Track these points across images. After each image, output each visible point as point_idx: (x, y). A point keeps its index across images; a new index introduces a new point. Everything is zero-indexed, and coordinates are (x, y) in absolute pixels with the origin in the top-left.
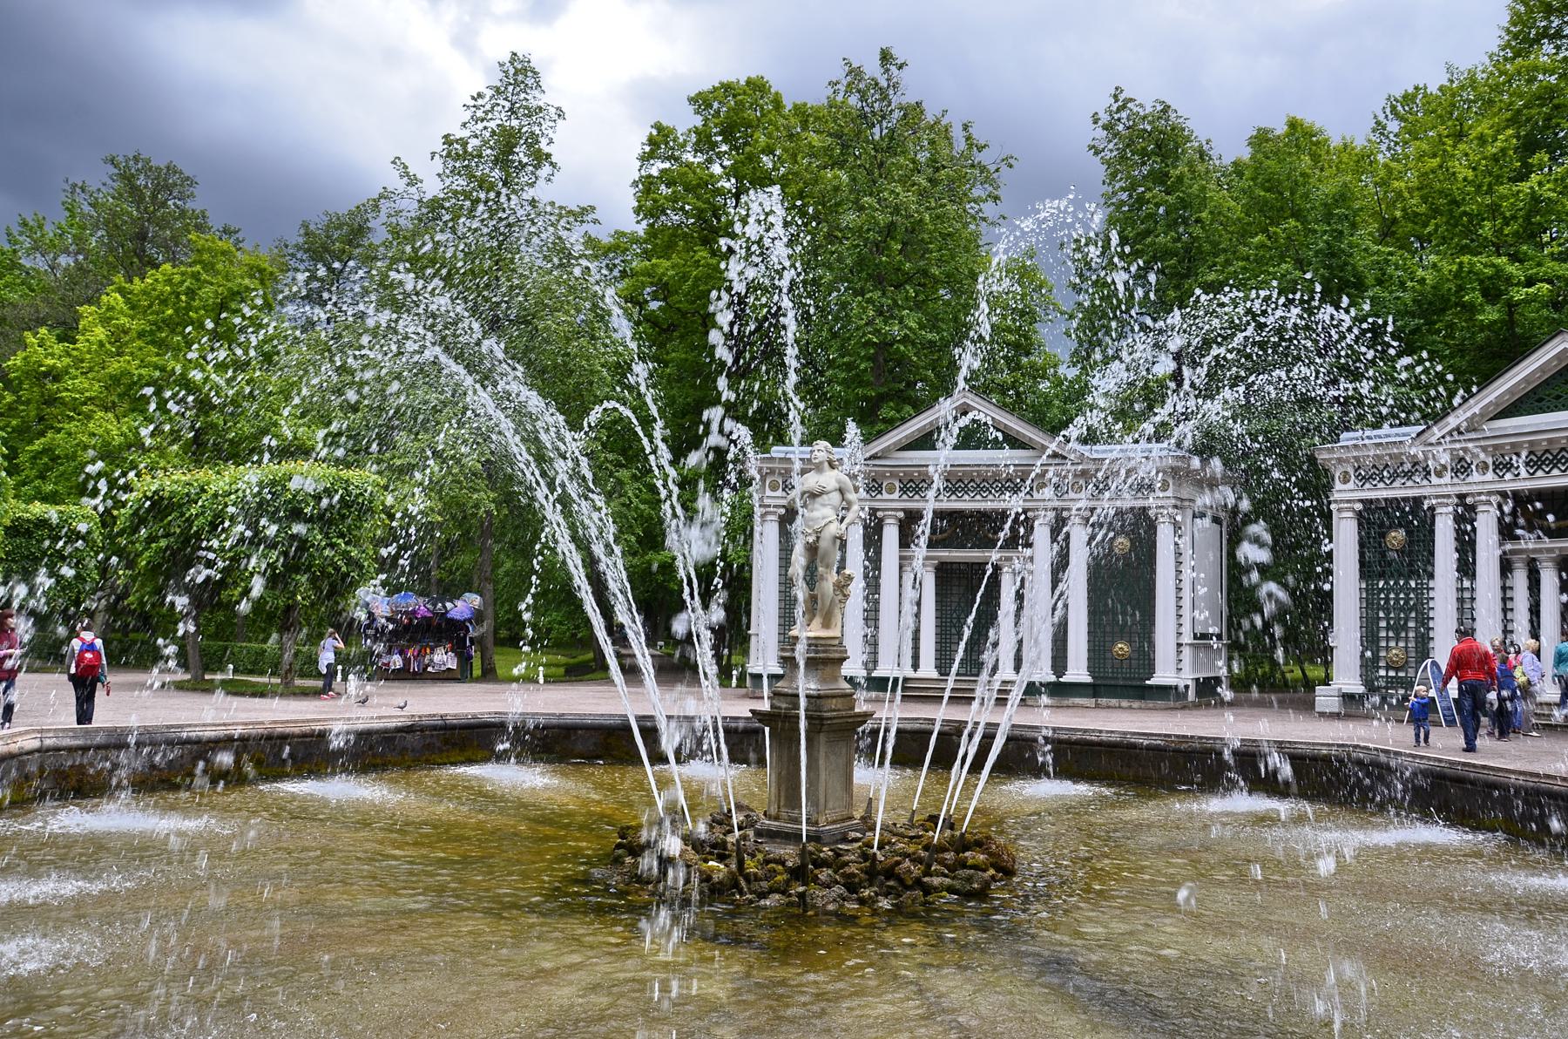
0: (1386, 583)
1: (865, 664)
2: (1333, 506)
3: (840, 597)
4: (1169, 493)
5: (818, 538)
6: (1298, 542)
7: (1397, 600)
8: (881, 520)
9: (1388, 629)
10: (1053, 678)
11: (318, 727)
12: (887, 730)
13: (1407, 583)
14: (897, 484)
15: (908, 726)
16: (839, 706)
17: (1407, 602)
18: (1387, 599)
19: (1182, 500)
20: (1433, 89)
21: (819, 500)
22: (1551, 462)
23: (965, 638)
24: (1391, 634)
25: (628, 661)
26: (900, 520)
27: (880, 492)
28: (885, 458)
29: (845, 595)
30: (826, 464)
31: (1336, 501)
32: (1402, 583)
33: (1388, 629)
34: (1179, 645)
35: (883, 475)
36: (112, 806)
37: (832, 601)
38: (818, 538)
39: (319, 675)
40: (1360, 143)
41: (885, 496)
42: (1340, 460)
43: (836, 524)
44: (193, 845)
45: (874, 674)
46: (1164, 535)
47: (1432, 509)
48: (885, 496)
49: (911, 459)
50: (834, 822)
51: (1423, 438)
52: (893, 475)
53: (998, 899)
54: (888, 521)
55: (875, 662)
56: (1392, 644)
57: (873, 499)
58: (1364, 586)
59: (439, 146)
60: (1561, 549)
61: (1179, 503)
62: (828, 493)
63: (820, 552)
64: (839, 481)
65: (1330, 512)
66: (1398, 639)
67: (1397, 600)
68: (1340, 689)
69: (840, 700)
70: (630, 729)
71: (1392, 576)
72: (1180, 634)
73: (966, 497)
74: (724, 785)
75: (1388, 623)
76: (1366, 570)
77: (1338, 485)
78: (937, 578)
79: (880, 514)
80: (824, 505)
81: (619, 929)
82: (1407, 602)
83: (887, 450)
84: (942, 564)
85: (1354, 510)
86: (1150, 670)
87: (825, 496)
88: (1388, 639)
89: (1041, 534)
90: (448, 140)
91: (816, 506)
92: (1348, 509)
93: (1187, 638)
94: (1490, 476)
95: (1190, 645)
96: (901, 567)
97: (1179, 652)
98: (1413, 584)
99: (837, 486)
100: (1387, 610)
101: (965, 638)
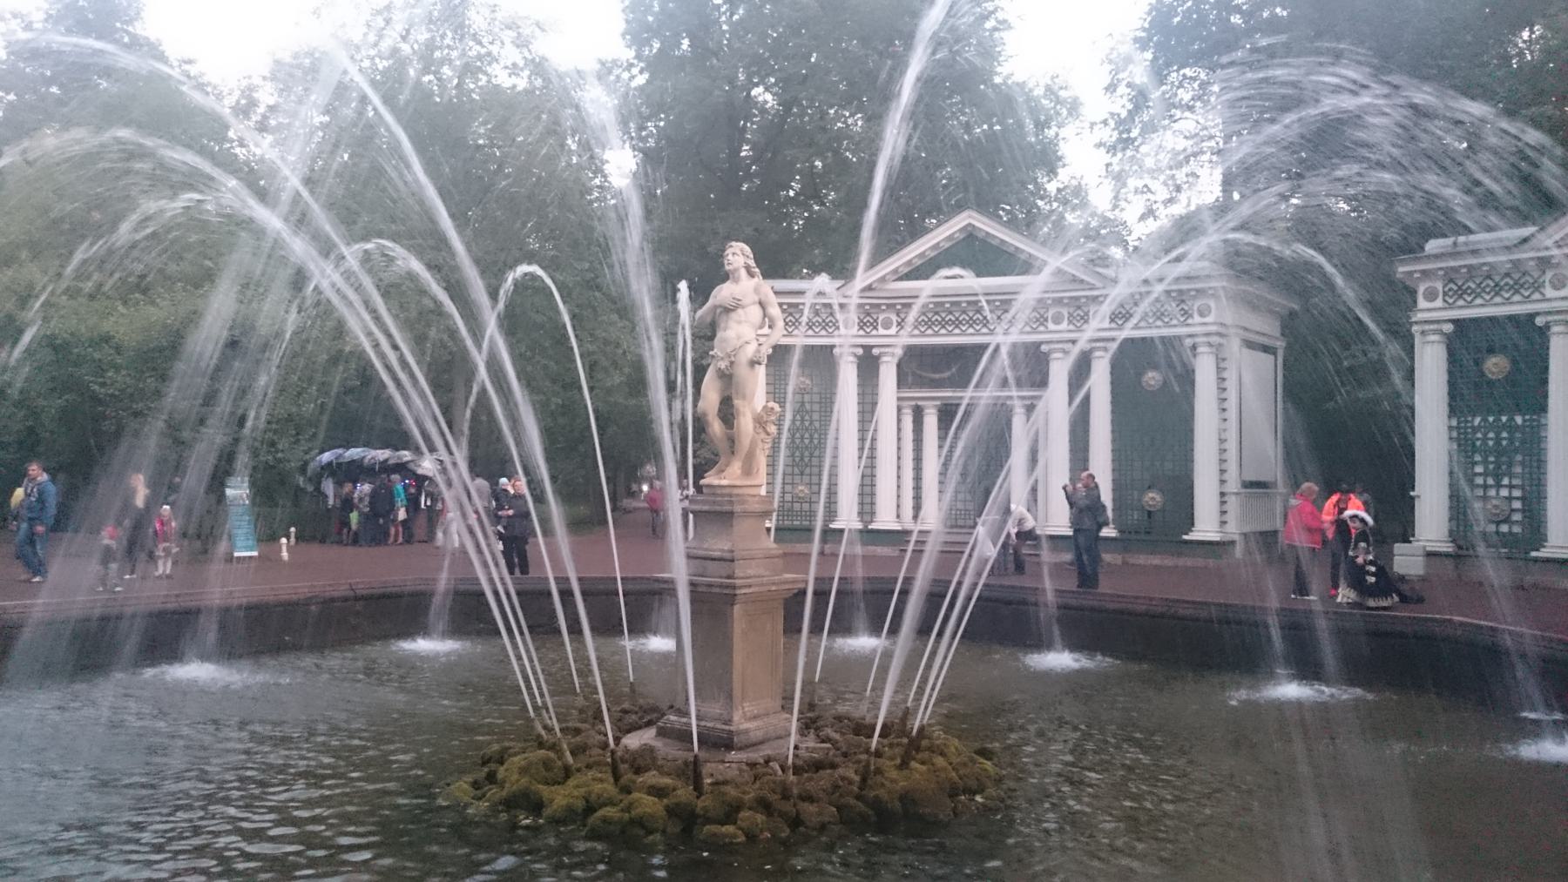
0: (1485, 420)
1: (861, 514)
2: (1415, 328)
8: (877, 358)
9: (1485, 474)
12: (905, 593)
13: (1511, 419)
15: (462, 588)
17: (802, 459)
18: (1485, 439)
21: (733, 315)
24: (1490, 481)
25: (583, 510)
27: (875, 328)
30: (743, 272)
31: (1416, 323)
32: (1504, 419)
33: (1485, 474)
34: (1222, 494)
36: (273, 662)
42: (1425, 274)
47: (1547, 326)
48: (881, 331)
50: (755, 717)
52: (889, 306)
53: (396, 762)
54: (1097, 354)
55: (873, 513)
56: (1492, 492)
57: (868, 335)
58: (1454, 423)
65: (1412, 337)
66: (1499, 486)
68: (1424, 547)
70: (593, 629)
71: (1489, 412)
72: (1223, 482)
73: (823, 333)
75: (1486, 468)
76: (1457, 403)
77: (1422, 303)
79: (875, 351)
80: (739, 322)
82: (802, 459)
85: (1441, 332)
86: (1190, 523)
87: (740, 311)
88: (1485, 487)
89: (1059, 371)
92: (1435, 332)
93: (1233, 485)
94: (1064, 325)
95: (1237, 494)
96: (899, 409)
97: (1223, 503)
98: (1519, 420)
100: (1486, 453)
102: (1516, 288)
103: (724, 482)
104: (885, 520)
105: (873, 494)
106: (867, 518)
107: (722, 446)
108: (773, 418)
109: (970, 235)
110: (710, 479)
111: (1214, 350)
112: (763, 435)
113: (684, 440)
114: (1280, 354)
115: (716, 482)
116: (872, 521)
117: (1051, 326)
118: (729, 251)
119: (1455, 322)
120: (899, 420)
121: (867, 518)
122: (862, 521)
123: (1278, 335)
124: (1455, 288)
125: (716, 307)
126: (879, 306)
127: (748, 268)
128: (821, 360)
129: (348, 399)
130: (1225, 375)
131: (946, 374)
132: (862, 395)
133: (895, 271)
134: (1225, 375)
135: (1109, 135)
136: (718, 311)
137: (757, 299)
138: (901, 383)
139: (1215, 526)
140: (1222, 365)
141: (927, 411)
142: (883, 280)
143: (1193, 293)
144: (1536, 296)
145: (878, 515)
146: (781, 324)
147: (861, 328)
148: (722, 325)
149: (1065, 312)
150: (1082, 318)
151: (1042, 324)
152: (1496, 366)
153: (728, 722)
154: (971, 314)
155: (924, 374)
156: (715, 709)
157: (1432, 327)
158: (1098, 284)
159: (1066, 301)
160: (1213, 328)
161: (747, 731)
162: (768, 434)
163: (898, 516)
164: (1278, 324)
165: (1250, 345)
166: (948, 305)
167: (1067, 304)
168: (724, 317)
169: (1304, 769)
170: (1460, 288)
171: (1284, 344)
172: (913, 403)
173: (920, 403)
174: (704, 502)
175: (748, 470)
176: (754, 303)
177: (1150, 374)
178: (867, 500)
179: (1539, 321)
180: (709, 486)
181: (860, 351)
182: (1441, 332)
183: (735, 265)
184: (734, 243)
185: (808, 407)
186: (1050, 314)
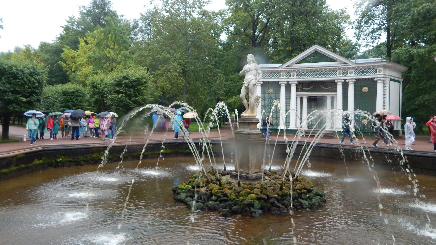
3: (256, 103)
4: (382, 73)
5: (249, 85)
6: (403, 211)
8: (291, 84)
11: (155, 132)
14: (295, 74)
16: (256, 137)
19: (386, 75)
21: (249, 73)
22: (366, 72)
23: (204, 119)
26: (261, 84)
27: (290, 76)
28: (292, 66)
29: (258, 103)
30: (252, 62)
35: (291, 71)
37: (254, 105)
38: (249, 85)
41: (292, 77)
42: (349, 68)
43: (254, 80)
45: (289, 128)
46: (380, 87)
48: (292, 77)
50: (254, 173)
51: (282, 67)
52: (294, 71)
55: (289, 125)
57: (288, 78)
61: (385, 76)
62: (251, 71)
63: (249, 89)
64: (255, 66)
69: (256, 135)
74: (213, 161)
79: (347, 81)
80: (251, 74)
83: (292, 64)
84: (309, 97)
85: (352, 81)
86: (278, 125)
91: (248, 75)
92: (339, 82)
96: (296, 98)
99: (255, 68)
101: (204, 119)
102: (276, 76)
103: (247, 115)
104: (292, 127)
105: (289, 120)
106: (287, 126)
109: (316, 53)
110: (243, 114)
111: (382, 81)
113: (248, 120)
114: (401, 83)
115: (244, 115)
117: (338, 75)
118: (248, 56)
119: (298, 81)
120: (296, 101)
123: (401, 77)
125: (245, 71)
126: (291, 70)
128: (277, 85)
129: (395, 51)
130: (385, 88)
132: (286, 94)
133: (295, 62)
134: (385, 88)
135: (356, 25)
136: (245, 71)
138: (297, 91)
140: (385, 86)
141: (304, 98)
143: (377, 66)
145: (290, 125)
146: (261, 75)
147: (286, 76)
148: (246, 75)
149: (342, 71)
150: (375, 71)
151: (335, 75)
152: (365, 89)
153: (248, 174)
154: (359, 70)
155: (303, 88)
156: (244, 171)
157: (351, 80)
158: (351, 64)
159: (352, 68)
160: (382, 76)
161: (252, 176)
163: (296, 126)
164: (401, 74)
165: (391, 80)
167: (342, 70)
168: (247, 73)
169: (271, 114)
170: (367, 71)
171: (402, 80)
172: (332, 96)
173: (333, 96)
174: (241, 120)
176: (254, 70)
177: (365, 88)
179: (375, 79)
180: (243, 116)
181: (343, 81)
182: (352, 81)
185: (272, 97)
186: (337, 72)
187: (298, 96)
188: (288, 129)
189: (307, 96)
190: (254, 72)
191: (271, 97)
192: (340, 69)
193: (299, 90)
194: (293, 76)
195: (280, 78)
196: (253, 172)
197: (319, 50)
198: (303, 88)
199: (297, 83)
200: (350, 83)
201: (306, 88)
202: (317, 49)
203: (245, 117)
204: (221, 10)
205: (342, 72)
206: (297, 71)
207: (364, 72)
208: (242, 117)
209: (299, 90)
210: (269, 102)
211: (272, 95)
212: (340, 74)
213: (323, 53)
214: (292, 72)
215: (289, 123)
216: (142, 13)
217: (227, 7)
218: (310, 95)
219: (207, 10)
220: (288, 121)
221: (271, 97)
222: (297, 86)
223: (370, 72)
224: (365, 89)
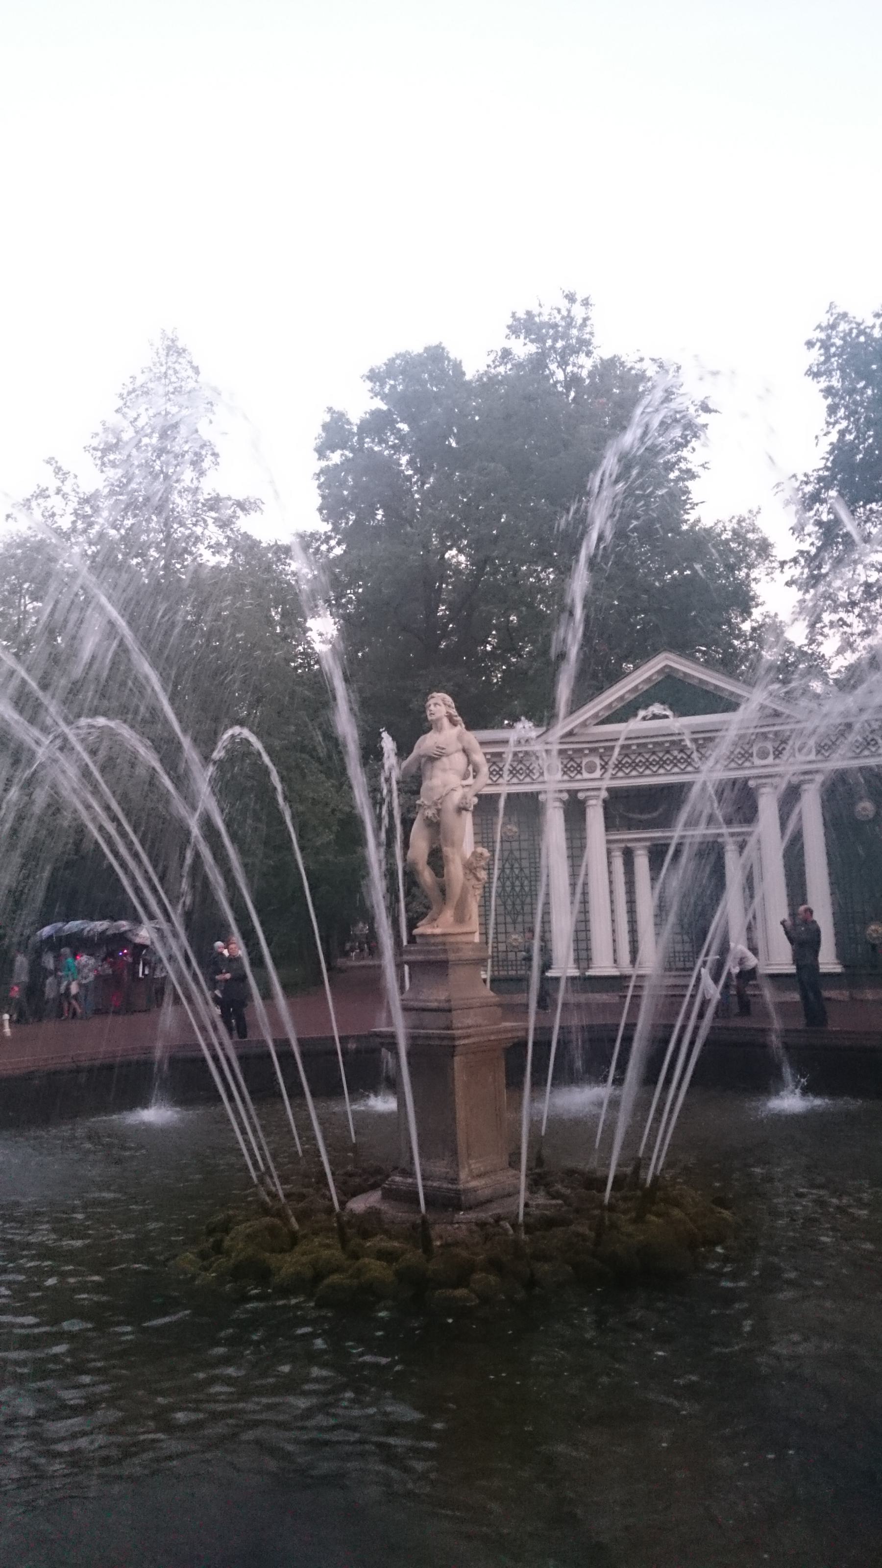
1: (577, 960)
5: (439, 811)
7: (513, 886)
10: (575, 973)
14: (598, 761)
20: (471, 372)
21: (438, 764)
27: (580, 772)
28: (582, 734)
30: (446, 721)
38: (439, 811)
39: (408, 963)
40: (774, 552)
44: (87, 1276)
45: (590, 973)
48: (586, 775)
49: (601, 734)
50: (480, 1176)
51: (543, 737)
55: (589, 959)
57: (572, 780)
59: (507, 331)
60: (654, 838)
64: (460, 738)
67: (513, 886)
78: (650, 861)
79: (581, 796)
80: (444, 770)
81: (86, 1379)
84: (656, 845)
87: (444, 759)
90: (509, 327)
96: (609, 852)
105: (588, 940)
106: (583, 964)
107: (434, 894)
108: (483, 863)
110: (424, 928)
112: (474, 882)
115: (429, 931)
116: (589, 968)
117: (757, 762)
118: (431, 702)
121: (583, 964)
122: (579, 968)
124: (575, 765)
126: (581, 750)
127: (450, 718)
131: (655, 814)
133: (596, 715)
137: (460, 746)
138: (610, 825)
139: (610, 962)
142: (584, 724)
144: (747, 764)
148: (428, 774)
150: (575, 769)
151: (747, 760)
155: (631, 815)
156: (440, 1167)
161: (475, 1190)
162: (478, 879)
163: (615, 961)
166: (650, 746)
172: (623, 845)
173: (629, 845)
175: (461, 918)
178: (583, 945)
183: (438, 715)
184: (435, 694)
185: (517, 854)
187: (614, 846)
188: (587, 974)
189: (648, 844)
190: (459, 760)
191: (511, 851)
192: (764, 736)
193: (617, 820)
194: (591, 769)
195: (541, 779)
196: (476, 1172)
197: (678, 670)
198: (631, 815)
199: (604, 794)
200: (592, 802)
201: (641, 813)
202: (670, 667)
203: (432, 941)
204: (811, 367)
205: (771, 750)
206: (602, 750)
207: (665, 762)
208: (418, 940)
209: (617, 820)
210: (508, 871)
211: (515, 845)
212: (763, 755)
213: (695, 682)
214: (586, 755)
215: (588, 949)
216: (518, 315)
217: (326, 527)
218: (659, 838)
219: (256, 536)
220: (583, 945)
221: (511, 851)
222: (606, 804)
223: (630, 765)
224: (864, 809)
